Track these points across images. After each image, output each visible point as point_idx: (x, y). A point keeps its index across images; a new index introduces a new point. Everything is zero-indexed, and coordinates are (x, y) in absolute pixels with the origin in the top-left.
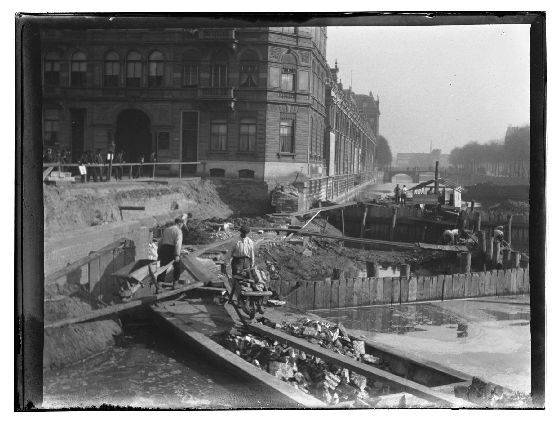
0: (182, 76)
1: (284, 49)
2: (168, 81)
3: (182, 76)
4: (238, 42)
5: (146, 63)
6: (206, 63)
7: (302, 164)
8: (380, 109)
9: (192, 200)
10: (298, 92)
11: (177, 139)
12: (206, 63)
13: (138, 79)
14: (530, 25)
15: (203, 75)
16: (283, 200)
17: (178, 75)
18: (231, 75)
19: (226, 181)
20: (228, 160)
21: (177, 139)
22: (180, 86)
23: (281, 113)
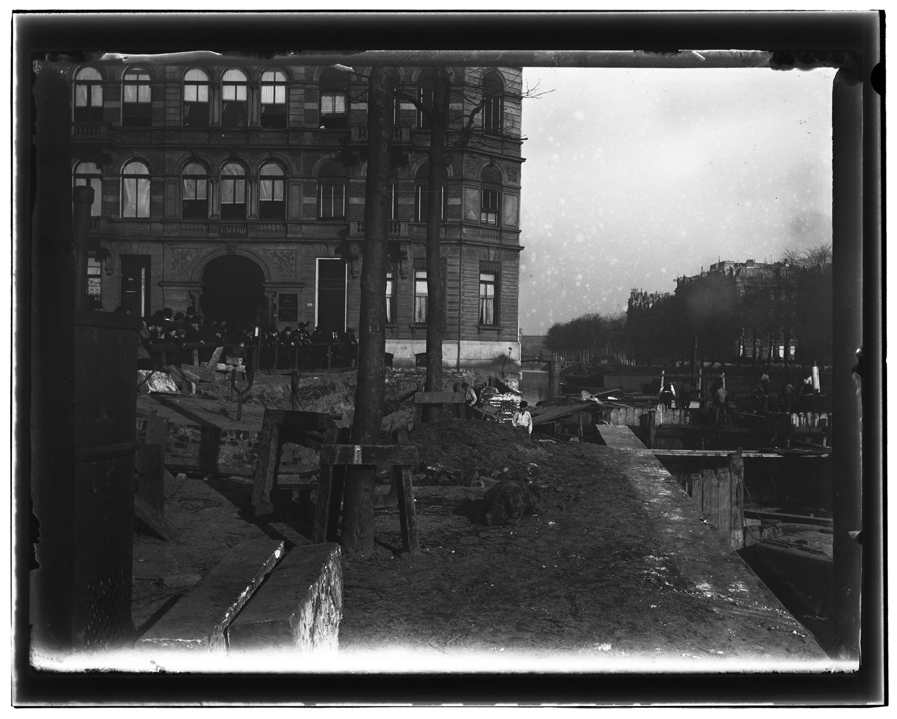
0: (319, 202)
1: (484, 159)
2: (294, 210)
3: (319, 202)
4: (151, 77)
5: (252, 179)
6: (359, 181)
7: (510, 343)
8: (523, 239)
9: (350, 404)
10: (504, 227)
11: (311, 305)
12: (359, 181)
13: (243, 207)
14: (831, 72)
15: (355, 201)
16: (498, 401)
17: (313, 200)
18: (401, 201)
19: (395, 373)
20: (398, 339)
21: (311, 305)
22: (315, 218)
23: (480, 261)
